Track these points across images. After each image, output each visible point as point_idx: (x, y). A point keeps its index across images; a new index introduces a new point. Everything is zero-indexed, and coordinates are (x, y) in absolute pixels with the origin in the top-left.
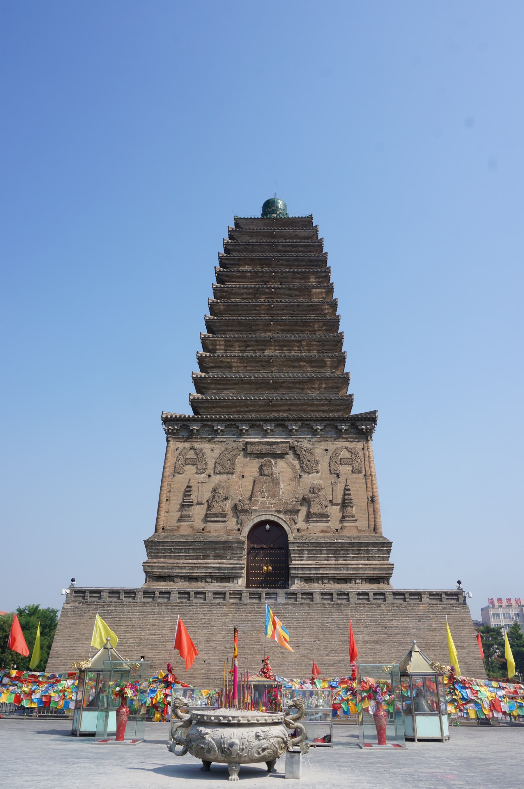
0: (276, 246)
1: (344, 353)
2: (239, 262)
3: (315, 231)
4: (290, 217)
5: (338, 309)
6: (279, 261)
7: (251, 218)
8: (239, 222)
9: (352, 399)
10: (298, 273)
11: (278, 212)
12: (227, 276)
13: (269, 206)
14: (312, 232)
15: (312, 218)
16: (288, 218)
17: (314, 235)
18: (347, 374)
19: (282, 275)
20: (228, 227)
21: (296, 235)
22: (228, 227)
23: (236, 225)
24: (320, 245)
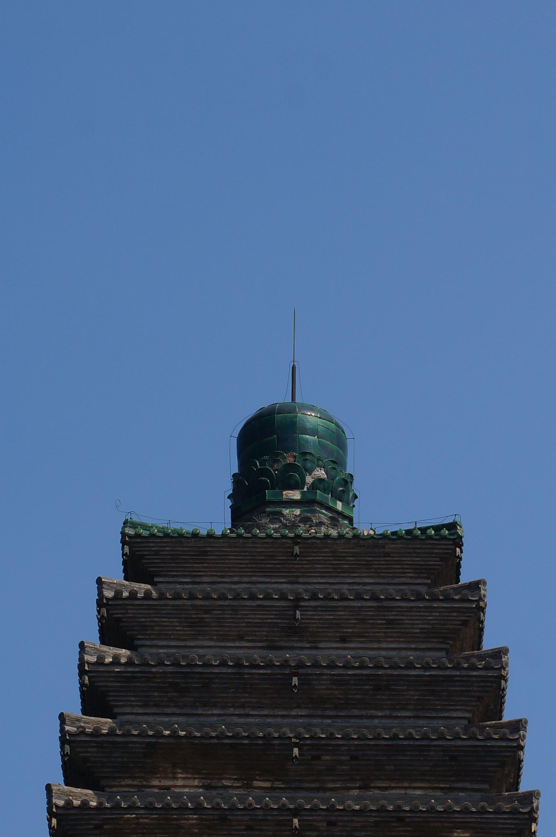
0: (305, 680)
1: (530, 796)
2: (153, 756)
3: (469, 607)
4: (366, 532)
5: (525, 766)
6: (317, 758)
7: (195, 535)
8: (147, 552)
9: (533, 811)
10: (401, 820)
11: (309, 480)
12: (98, 827)
13: (269, 448)
14: (458, 610)
15: (458, 542)
16: (356, 537)
17: (465, 623)
18: (518, 726)
19: (331, 824)
20: (99, 581)
21: (390, 622)
22: (99, 581)
23: (133, 568)
24: (488, 681)
